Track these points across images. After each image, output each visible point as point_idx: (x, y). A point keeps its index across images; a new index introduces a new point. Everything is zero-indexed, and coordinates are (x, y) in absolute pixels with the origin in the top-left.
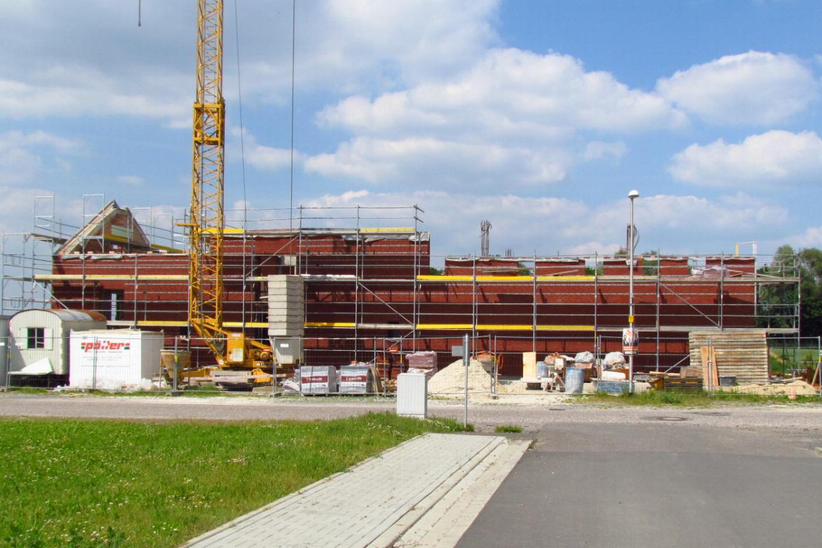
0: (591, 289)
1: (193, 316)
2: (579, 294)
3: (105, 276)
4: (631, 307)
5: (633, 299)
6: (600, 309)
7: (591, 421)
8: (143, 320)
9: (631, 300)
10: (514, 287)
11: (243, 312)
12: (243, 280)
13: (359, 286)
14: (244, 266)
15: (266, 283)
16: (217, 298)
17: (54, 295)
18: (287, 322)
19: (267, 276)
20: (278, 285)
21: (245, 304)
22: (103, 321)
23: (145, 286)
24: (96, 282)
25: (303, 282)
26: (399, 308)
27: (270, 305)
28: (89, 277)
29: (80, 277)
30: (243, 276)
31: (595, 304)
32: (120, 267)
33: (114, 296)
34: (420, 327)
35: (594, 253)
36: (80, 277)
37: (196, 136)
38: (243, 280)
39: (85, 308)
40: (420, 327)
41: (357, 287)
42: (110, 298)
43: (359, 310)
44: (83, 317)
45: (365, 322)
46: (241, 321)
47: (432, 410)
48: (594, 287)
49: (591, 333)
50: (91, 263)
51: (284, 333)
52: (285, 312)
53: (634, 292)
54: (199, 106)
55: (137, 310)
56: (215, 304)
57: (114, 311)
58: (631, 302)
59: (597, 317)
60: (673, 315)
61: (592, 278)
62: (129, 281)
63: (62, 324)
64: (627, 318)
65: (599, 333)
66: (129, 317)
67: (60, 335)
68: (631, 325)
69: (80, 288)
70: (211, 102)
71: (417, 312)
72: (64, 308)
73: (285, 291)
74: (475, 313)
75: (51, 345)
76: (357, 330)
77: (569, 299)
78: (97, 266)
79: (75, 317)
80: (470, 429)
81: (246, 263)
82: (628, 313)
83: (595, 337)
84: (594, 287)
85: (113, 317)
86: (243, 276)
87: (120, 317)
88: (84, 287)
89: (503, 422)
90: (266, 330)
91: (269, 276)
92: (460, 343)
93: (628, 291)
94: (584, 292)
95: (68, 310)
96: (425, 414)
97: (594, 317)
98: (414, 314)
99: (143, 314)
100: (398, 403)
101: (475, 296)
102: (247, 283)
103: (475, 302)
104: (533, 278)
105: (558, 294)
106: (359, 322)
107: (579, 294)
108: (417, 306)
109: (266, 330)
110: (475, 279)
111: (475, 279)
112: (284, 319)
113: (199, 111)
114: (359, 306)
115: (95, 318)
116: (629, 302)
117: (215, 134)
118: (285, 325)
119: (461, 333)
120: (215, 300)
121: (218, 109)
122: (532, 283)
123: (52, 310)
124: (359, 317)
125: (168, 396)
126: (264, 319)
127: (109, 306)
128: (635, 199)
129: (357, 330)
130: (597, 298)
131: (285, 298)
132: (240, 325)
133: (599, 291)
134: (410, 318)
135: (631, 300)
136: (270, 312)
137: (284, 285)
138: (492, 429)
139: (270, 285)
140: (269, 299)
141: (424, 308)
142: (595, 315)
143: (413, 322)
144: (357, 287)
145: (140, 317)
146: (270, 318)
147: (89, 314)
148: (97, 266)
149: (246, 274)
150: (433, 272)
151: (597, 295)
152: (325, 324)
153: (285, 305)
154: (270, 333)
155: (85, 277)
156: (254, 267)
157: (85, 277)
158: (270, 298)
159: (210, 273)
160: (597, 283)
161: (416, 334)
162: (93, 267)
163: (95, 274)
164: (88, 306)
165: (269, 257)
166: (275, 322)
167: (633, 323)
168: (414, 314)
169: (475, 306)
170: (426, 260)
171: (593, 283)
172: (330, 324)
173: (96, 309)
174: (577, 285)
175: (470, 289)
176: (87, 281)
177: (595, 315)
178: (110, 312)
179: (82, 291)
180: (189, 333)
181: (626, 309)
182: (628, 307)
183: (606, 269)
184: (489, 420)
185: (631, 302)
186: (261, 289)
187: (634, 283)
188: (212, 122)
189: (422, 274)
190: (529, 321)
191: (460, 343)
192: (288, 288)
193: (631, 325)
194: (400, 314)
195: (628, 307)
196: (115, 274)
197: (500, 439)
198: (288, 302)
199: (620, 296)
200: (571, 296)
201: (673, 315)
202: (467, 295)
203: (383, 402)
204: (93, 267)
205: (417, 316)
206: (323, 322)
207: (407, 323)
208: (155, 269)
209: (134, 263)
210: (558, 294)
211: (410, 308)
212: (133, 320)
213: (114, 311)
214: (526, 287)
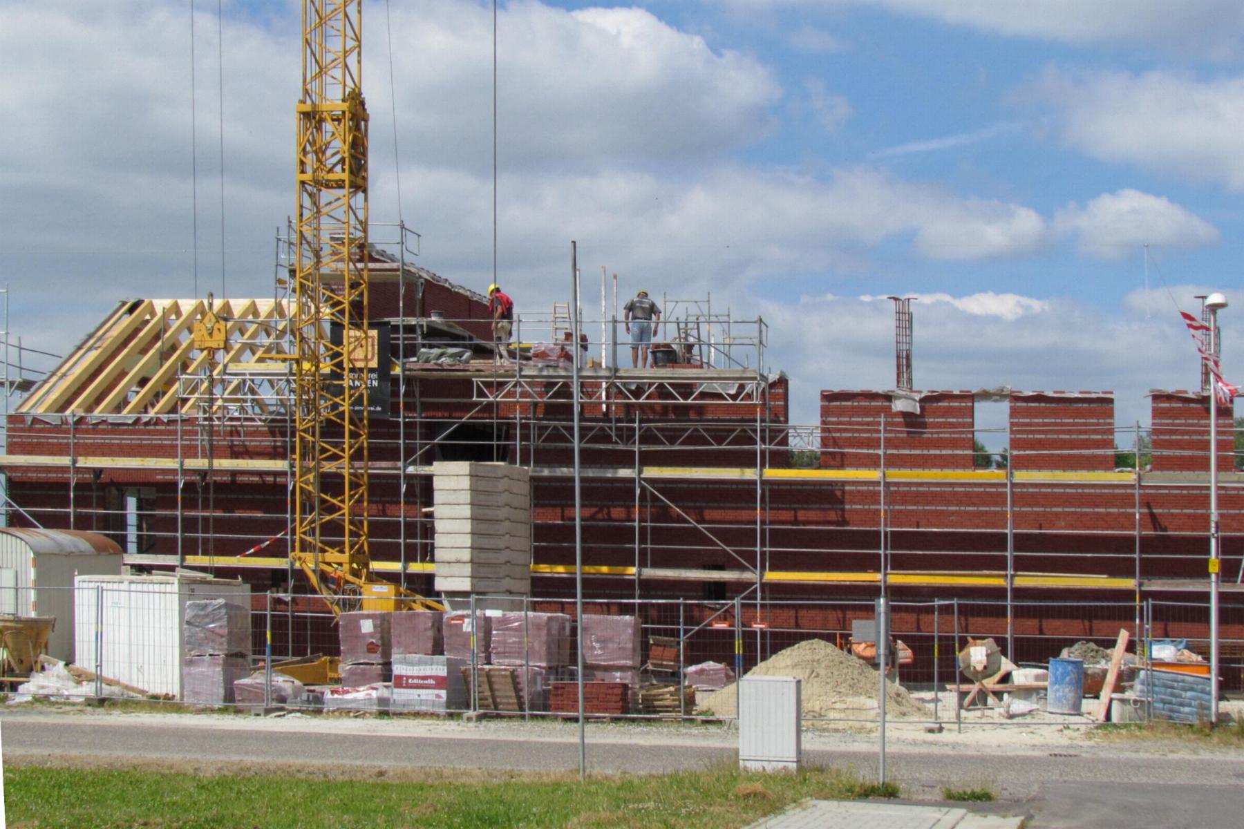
0: (1127, 500)
1: (305, 547)
2: (1102, 510)
3: (694, 469)
4: (1213, 542)
5: (1217, 523)
6: (1148, 544)
7: (1135, 780)
8: (196, 553)
9: (1213, 525)
10: (967, 493)
11: (402, 541)
12: (401, 472)
13: (643, 489)
14: (401, 441)
15: (429, 479)
16: (346, 511)
17: (11, 496)
18: (472, 561)
19: (431, 464)
20: (452, 483)
21: (406, 523)
22: (115, 553)
23: (897, 493)
24: (98, 472)
25: (527, 479)
26: (727, 537)
27: (439, 526)
28: (83, 462)
29: (65, 461)
30: (401, 464)
31: (1136, 533)
32: (146, 440)
33: (132, 502)
34: (772, 576)
35: (1134, 424)
36: (65, 461)
37: (303, 172)
38: (401, 472)
39: (77, 527)
40: (772, 576)
41: (638, 491)
42: (123, 506)
43: (643, 540)
44: (75, 546)
45: (655, 565)
46: (397, 559)
47: (808, 753)
48: (1133, 495)
49: (1128, 595)
50: (87, 432)
51: (465, 585)
52: (467, 541)
53: (1219, 506)
54: (307, 108)
55: (651, 549)
56: (344, 520)
57: (132, 533)
58: (1213, 530)
59: (1141, 560)
60: (1089, 555)
61: (1127, 477)
62: (276, 474)
63: (34, 559)
64: (1206, 562)
65: (1145, 595)
66: (167, 547)
67: (31, 585)
68: (1213, 577)
69: (65, 485)
70: (334, 98)
71: (763, 545)
72: (36, 527)
73: (466, 497)
74: (886, 548)
75: (12, 601)
76: (886, 588)
77: (1080, 520)
78: (99, 439)
79: (59, 544)
80: (888, 793)
81: (407, 436)
82: (1208, 552)
83: (1137, 603)
84: (1133, 495)
85: (132, 547)
86: (401, 464)
87: (145, 546)
88: (73, 485)
89: (958, 780)
90: (430, 578)
91: (435, 463)
92: (870, 610)
93: (1208, 506)
94: (1113, 506)
95: (42, 530)
96: (798, 761)
97: (1134, 559)
98: (758, 549)
99: (196, 540)
100: (740, 740)
101: (886, 511)
102: (409, 477)
103: (886, 526)
104: (80, 464)
105: (1060, 509)
106: (643, 564)
107: (1102, 510)
108: (763, 531)
109: (430, 578)
110: (182, 465)
111: (182, 465)
112: (466, 555)
113: (312, 118)
114: (643, 530)
115: (100, 549)
116: (1208, 528)
117: (339, 166)
118: (467, 569)
119: (872, 591)
120: (343, 515)
121: (344, 112)
122: (878, 483)
123: (11, 530)
124: (643, 552)
125: (258, 715)
126: (428, 553)
127: (121, 523)
128: (1220, 311)
129: (886, 588)
130: (1141, 519)
131: (466, 511)
132: (396, 567)
133: (1147, 503)
134: (751, 557)
135: (1213, 525)
136: (439, 540)
137: (466, 483)
138: (937, 795)
139: (437, 483)
140: (436, 515)
141: (777, 538)
142: (1136, 556)
143: (755, 567)
144: (638, 491)
145: (190, 548)
146: (439, 554)
147: (88, 540)
148: (99, 439)
149: (405, 460)
150: (983, 461)
151: (1141, 514)
152: (605, 569)
153: (467, 526)
154: (440, 585)
155: (75, 462)
156: (422, 446)
157: (75, 462)
158: (437, 510)
159: (335, 457)
160: (1141, 487)
161: (763, 591)
162: (90, 439)
163: (94, 454)
164: (83, 523)
165: (455, 423)
166: (449, 563)
167: (1217, 575)
168: (758, 549)
169: (886, 533)
170: (778, 434)
171: (1132, 486)
172: (619, 569)
173: (98, 529)
174: (1098, 491)
175: (873, 497)
176: (79, 470)
177: (1136, 556)
178: (125, 536)
179: (69, 490)
180: (291, 583)
181: (1203, 545)
182: (1207, 540)
183: (1160, 457)
184: (926, 775)
185: (1213, 530)
186: (424, 490)
187: (1219, 488)
188: (337, 142)
189: (772, 466)
190: (871, 564)
191: (870, 610)
192: (473, 490)
193: (1213, 577)
194: (728, 549)
195: (1207, 541)
196: (135, 456)
197: (957, 812)
198: (473, 519)
199: (1189, 516)
200: (1086, 514)
201: (1089, 555)
202: (868, 511)
203: (404, 705)
204: (90, 439)
205: (763, 553)
206: (602, 564)
207: (742, 568)
208: (141, 446)
209: (175, 433)
210: (1060, 509)
211: (749, 538)
212: (175, 553)
213: (132, 533)
214: (991, 494)
